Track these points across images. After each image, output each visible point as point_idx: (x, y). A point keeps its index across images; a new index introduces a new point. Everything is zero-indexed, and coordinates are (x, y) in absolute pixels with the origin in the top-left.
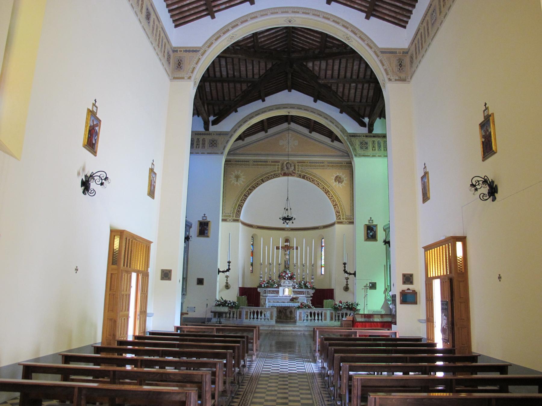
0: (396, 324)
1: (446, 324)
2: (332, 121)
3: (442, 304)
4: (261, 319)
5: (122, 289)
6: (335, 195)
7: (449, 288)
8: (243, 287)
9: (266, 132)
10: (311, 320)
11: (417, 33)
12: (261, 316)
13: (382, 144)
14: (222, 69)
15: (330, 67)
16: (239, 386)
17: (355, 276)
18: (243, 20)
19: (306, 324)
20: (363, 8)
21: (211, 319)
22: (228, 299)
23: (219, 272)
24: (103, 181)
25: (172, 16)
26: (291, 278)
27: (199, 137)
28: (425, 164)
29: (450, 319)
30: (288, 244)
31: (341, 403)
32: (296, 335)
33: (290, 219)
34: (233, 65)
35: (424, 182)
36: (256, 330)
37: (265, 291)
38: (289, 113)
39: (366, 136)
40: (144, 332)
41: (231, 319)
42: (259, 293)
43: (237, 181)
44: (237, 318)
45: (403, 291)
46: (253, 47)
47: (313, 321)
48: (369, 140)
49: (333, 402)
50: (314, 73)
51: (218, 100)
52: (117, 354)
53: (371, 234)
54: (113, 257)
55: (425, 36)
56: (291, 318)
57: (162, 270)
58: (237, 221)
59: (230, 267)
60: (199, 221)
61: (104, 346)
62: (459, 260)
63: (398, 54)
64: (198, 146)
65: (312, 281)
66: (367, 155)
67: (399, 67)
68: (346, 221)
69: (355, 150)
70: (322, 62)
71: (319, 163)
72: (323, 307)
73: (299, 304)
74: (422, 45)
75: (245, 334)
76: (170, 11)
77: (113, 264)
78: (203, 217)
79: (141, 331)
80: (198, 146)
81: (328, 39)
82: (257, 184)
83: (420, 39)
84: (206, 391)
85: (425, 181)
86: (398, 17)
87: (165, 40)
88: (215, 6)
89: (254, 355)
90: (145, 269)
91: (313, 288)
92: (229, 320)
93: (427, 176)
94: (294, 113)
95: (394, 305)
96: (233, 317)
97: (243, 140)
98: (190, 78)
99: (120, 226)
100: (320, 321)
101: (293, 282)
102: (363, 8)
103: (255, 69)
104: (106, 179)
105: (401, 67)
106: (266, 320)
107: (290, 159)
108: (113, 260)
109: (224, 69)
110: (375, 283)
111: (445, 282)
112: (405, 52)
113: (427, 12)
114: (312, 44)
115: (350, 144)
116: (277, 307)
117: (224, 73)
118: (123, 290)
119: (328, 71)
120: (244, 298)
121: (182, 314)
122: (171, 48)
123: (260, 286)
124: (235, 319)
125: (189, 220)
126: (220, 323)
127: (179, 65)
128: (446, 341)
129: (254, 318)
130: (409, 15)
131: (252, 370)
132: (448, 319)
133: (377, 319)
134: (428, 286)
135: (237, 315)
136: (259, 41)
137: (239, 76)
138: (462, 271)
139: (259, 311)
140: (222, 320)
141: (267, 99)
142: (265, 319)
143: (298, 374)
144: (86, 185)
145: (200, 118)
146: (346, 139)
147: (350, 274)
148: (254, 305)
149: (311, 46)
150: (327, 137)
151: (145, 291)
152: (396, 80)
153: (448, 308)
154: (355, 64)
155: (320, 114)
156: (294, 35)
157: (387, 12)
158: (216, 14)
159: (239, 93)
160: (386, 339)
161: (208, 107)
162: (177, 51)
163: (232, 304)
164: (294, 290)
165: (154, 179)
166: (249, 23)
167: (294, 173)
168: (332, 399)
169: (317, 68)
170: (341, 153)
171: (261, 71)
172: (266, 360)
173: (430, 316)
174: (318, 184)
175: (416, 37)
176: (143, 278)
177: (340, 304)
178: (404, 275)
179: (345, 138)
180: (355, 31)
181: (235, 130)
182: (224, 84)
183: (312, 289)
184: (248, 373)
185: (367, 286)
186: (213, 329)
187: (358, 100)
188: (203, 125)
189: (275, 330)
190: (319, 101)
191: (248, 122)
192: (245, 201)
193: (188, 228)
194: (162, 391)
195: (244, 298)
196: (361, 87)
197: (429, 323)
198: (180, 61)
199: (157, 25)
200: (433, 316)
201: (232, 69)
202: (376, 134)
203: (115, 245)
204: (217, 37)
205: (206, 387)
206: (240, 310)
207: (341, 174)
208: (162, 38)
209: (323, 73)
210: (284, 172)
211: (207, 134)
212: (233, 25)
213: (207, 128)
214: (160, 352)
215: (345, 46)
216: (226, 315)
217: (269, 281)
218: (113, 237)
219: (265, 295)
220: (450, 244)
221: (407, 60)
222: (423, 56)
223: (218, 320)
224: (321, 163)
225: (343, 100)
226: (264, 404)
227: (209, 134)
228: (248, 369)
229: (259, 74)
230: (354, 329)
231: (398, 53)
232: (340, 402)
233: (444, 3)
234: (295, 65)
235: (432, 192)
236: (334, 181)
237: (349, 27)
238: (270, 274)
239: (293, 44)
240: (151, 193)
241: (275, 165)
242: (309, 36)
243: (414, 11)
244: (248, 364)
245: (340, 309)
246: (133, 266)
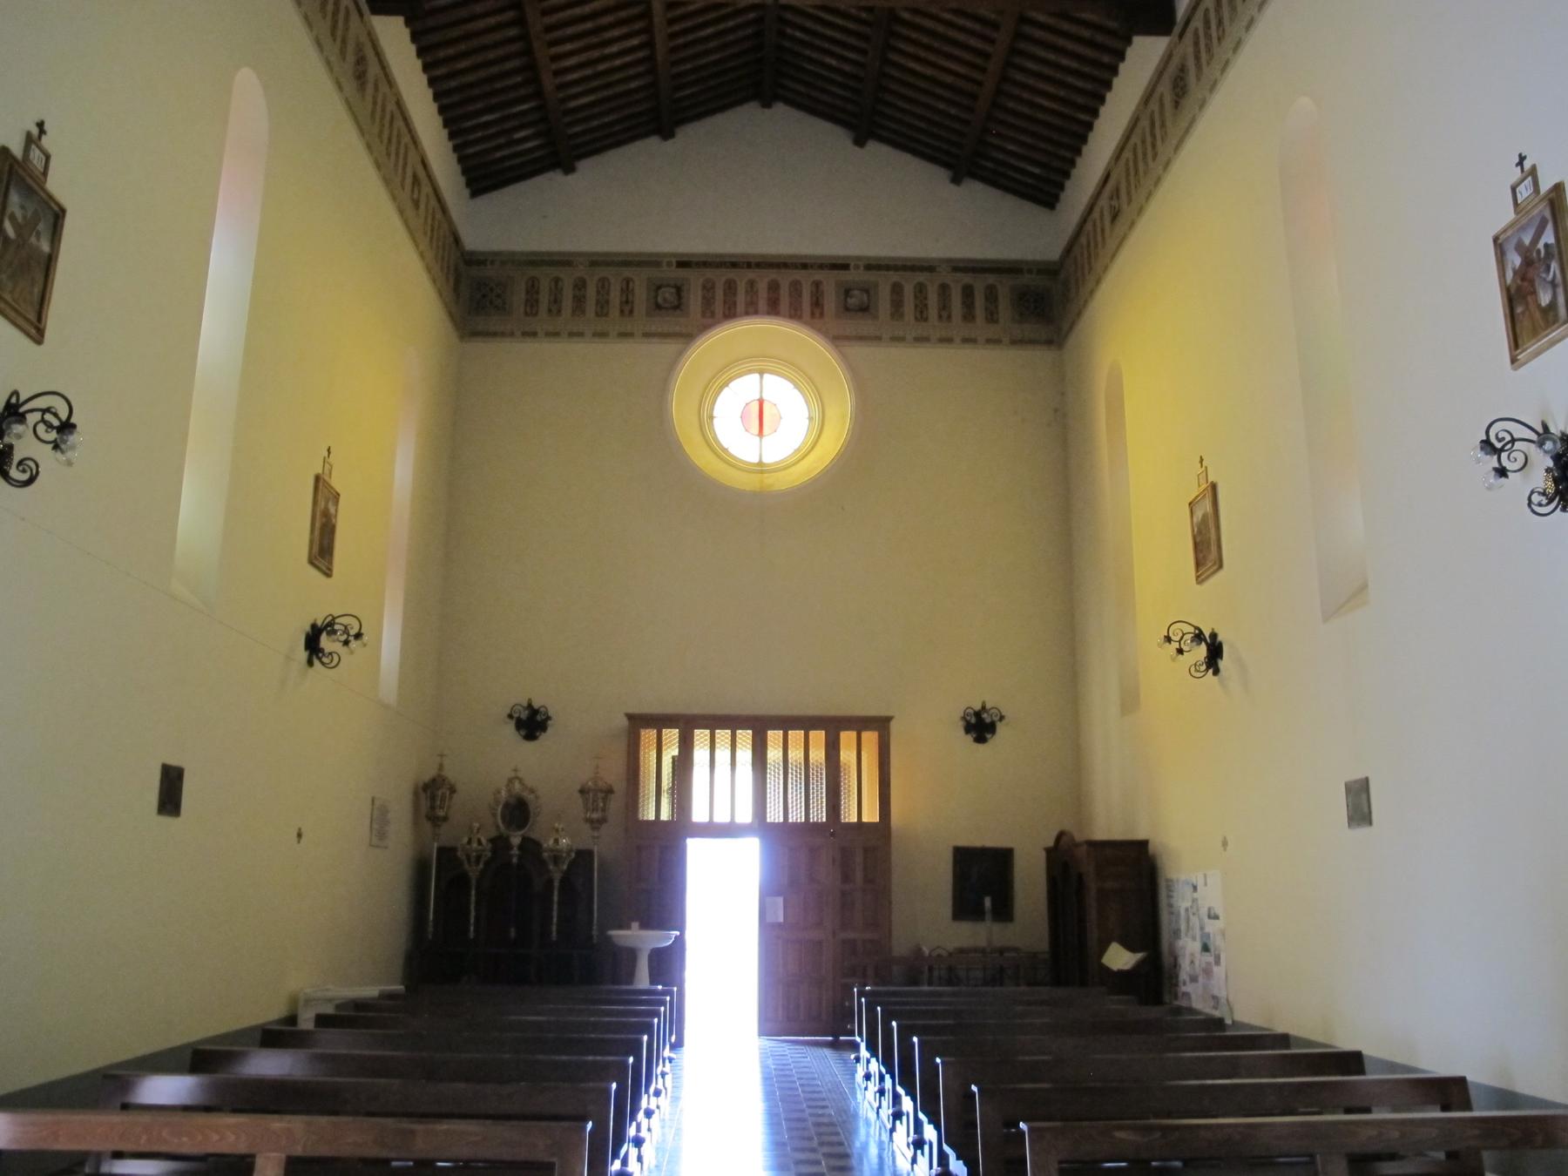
24: (351, 638)
28: (1202, 460)
83: (1148, 130)
87: (406, 139)
144: (313, 643)
233: (1221, 32)
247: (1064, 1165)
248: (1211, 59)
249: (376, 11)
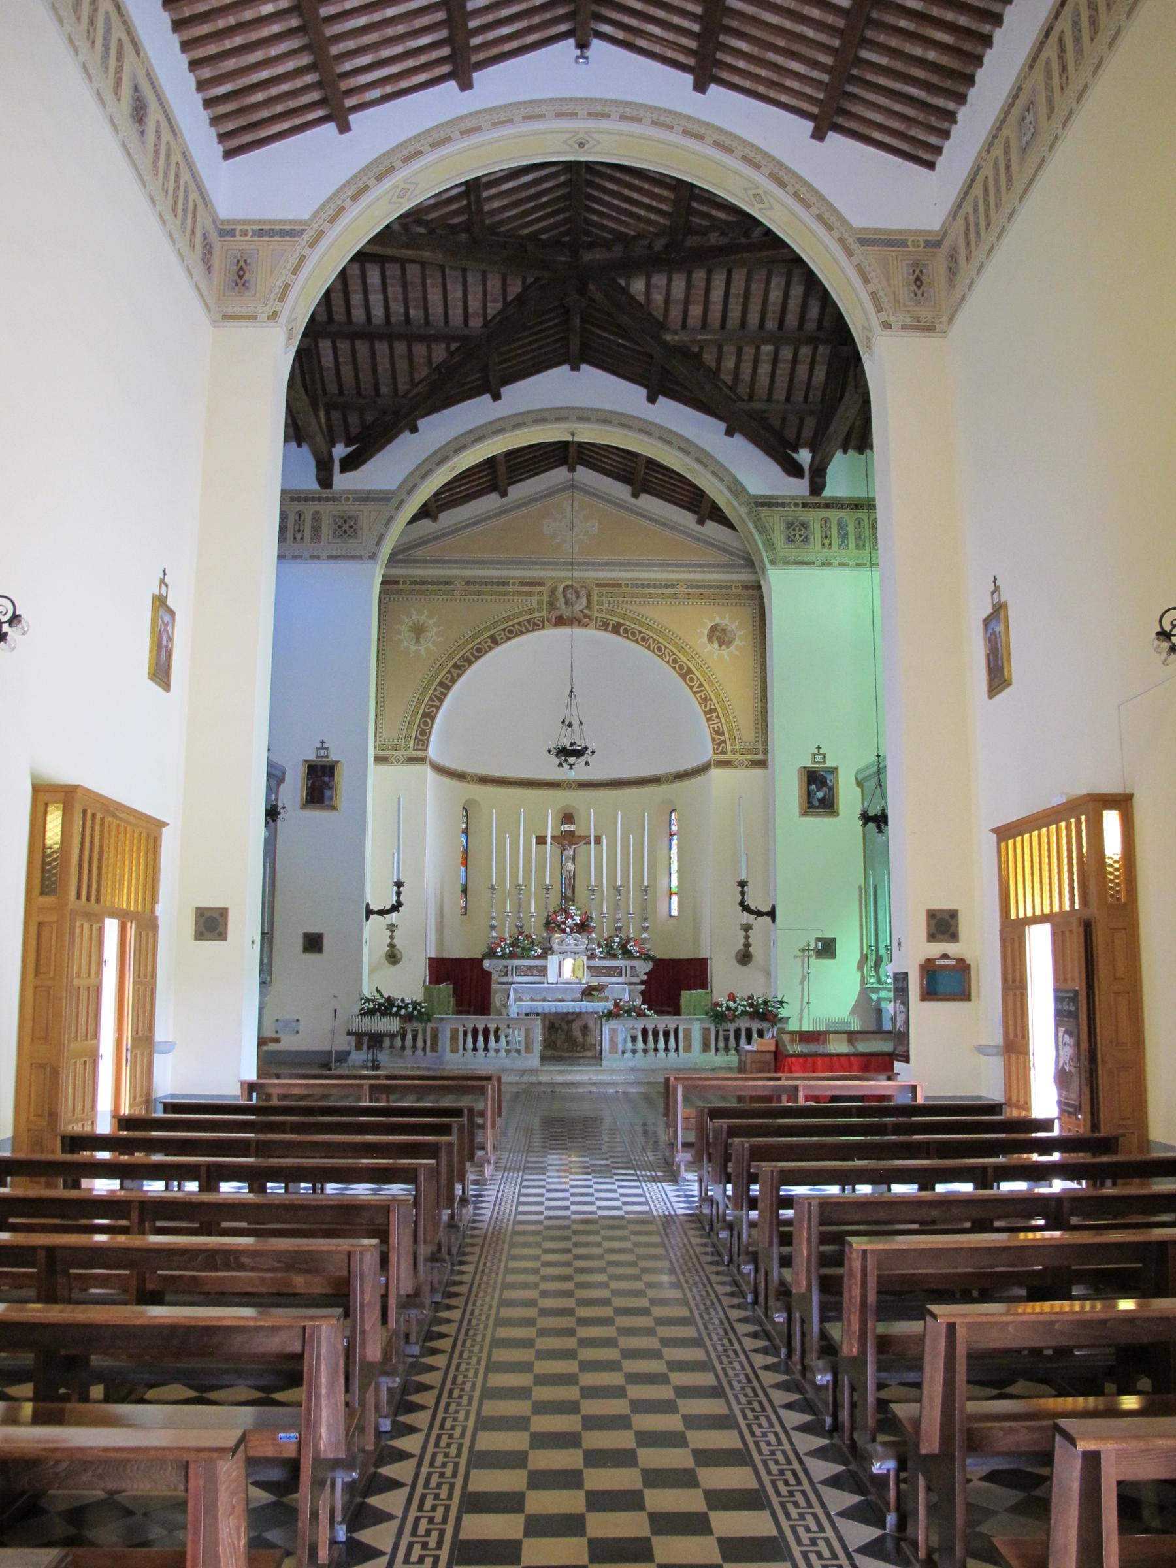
0: (907, 1060)
1: (1071, 1059)
2: (704, 458)
3: (1059, 999)
4: (497, 1051)
5: (76, 970)
6: (710, 683)
7: (1082, 950)
8: (440, 956)
9: (504, 494)
10: (645, 1051)
11: (973, 180)
12: (497, 1040)
13: (851, 529)
14: (372, 297)
15: (698, 293)
16: (453, 1264)
17: (774, 920)
18: (439, 137)
19: (630, 1064)
20: (805, 106)
21: (348, 1053)
22: (396, 995)
23: (369, 912)
25: (215, 121)
26: (583, 927)
27: (300, 507)
28: (995, 579)
29: (1085, 1045)
30: (572, 827)
31: (789, 1319)
32: (604, 1098)
33: (578, 753)
34: (405, 286)
35: (994, 633)
36: (493, 1086)
37: (506, 967)
38: (573, 434)
39: (804, 505)
40: (148, 1101)
41: (408, 1052)
42: (489, 974)
43: (418, 641)
44: (424, 1049)
45: (928, 961)
46: (467, 227)
47: (652, 1053)
48: (814, 517)
49: (754, 1310)
50: (650, 314)
51: (359, 393)
52: (61, 1181)
53: (820, 795)
54: (43, 871)
55: (998, 190)
56: (585, 1047)
57: (198, 909)
58: (420, 760)
59: (402, 899)
60: (306, 761)
61: (22, 1156)
62: (1111, 866)
63: (911, 249)
64: (298, 536)
65: (645, 935)
66: (806, 560)
67: (914, 288)
68: (743, 757)
69: (770, 545)
70: (675, 276)
71: (660, 586)
72: (679, 1014)
73: (610, 1005)
74: (987, 215)
75: (464, 1102)
76: (208, 103)
77: (42, 893)
78: (318, 749)
79: (138, 1099)
80: (298, 536)
81: (695, 205)
82: (479, 650)
84: (362, 1305)
85: (997, 630)
86: (913, 132)
87: (194, 196)
88: (350, 92)
89: (489, 1162)
90: (144, 906)
91: (646, 957)
92: (401, 1057)
93: (1002, 615)
94: (589, 434)
95: (902, 1003)
96: (414, 1047)
97: (435, 519)
98: (274, 316)
99: (64, 773)
100: (672, 1054)
101: (589, 939)
102: (805, 106)
103: (470, 297)
104: (15, 621)
105: (919, 287)
106: (514, 1054)
107: (576, 574)
108: (43, 879)
109: (376, 299)
110: (833, 940)
111: (1067, 933)
112: (933, 243)
113: (1007, 113)
114: (649, 222)
115: (756, 526)
116: (545, 1014)
117: (378, 312)
118: (79, 973)
119: (691, 307)
120: (446, 988)
121: (262, 1041)
122: (214, 222)
123: (491, 954)
124: (419, 1052)
125: (275, 759)
126: (376, 1067)
127: (241, 277)
128: (1070, 1109)
129: (475, 1049)
130: (945, 125)
131: (487, 1211)
132: (1078, 1044)
133: (838, 1046)
134: (1009, 945)
135: (425, 1042)
136: (486, 208)
137: (422, 321)
138: (1119, 899)
139: (492, 1027)
140: (383, 1057)
141: (506, 391)
142: (508, 1051)
143: (630, 1222)
145: (305, 450)
146: (744, 515)
147: (759, 914)
148: (472, 1009)
149: (642, 225)
150: (683, 511)
151: (145, 976)
152: (904, 327)
153: (1077, 1009)
154: (772, 285)
155: (667, 437)
156: (589, 190)
157: (878, 117)
158: (352, 118)
159: (424, 374)
160: (879, 1106)
161: (327, 414)
162: (231, 233)
163: (410, 1010)
164: (592, 963)
165: (169, 628)
166: (458, 147)
167: (586, 616)
168: (749, 1300)
169: (658, 297)
170: (725, 558)
171: (489, 305)
172: (526, 1177)
173: (1016, 1036)
174: (659, 649)
175: (966, 193)
176: (139, 934)
177: (731, 1004)
178: (932, 915)
179: (743, 510)
180: (781, 175)
181: (409, 484)
182: (377, 345)
183: (645, 960)
184: (475, 1221)
185: (808, 950)
186: (361, 1086)
187: (780, 395)
188: (314, 471)
189: (540, 1083)
190: (662, 399)
191: (451, 463)
192: (441, 701)
193: (273, 783)
194: (219, 1323)
195: (446, 988)
196: (790, 357)
197: (1013, 1056)
198: (242, 263)
199: (168, 143)
200: (1025, 1036)
201: (400, 297)
202: (832, 498)
203: (48, 834)
204: (357, 188)
205: (362, 1292)
206: (434, 1025)
207: (726, 621)
208: (186, 187)
209: (675, 313)
210: (558, 613)
211: (327, 499)
212: (406, 153)
213: (325, 481)
214: (203, 1170)
215: (747, 221)
216: (392, 1042)
217: (517, 939)
218: (41, 808)
219: (504, 979)
220: (1083, 818)
221: (938, 268)
222: (992, 248)
223: (370, 1057)
224: (666, 586)
225: (736, 394)
226: (539, 1326)
227: (333, 499)
228: (476, 1208)
229: (485, 315)
230: (788, 1079)
231: (909, 244)
232: (785, 1315)
233: (1064, 79)
234: (591, 287)
235: (1018, 666)
236: (705, 639)
237: (763, 162)
238: (519, 918)
239: (588, 221)
240: (161, 673)
241: (530, 594)
242: (636, 196)
243: (963, 113)
244: (472, 1190)
245: (729, 1014)
246: (109, 898)
247: (888, 1298)
248: (1096, 33)
249: (775, 1538)
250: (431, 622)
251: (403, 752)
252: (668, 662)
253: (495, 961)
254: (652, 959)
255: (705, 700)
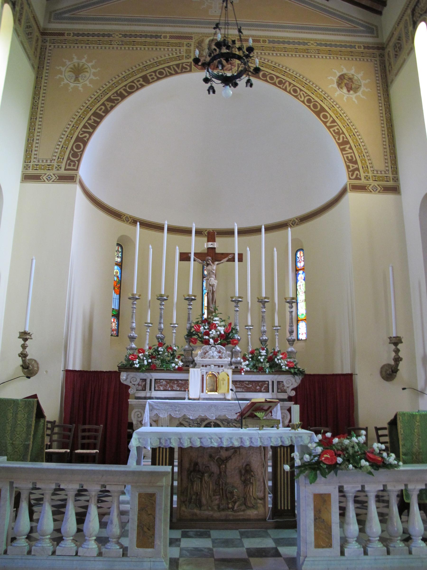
37: (145, 380)
43: (76, 79)
58: (71, 179)
68: (376, 183)
82: (131, 87)
164: (238, 377)
170: (348, 25)
174: (295, 91)
192: (94, 128)
207: (352, 72)
217: (157, 351)
219: (142, 394)
224: (299, 43)
236: (335, 85)
238: (160, 330)
241: (180, 45)
250: (90, 64)
251: (55, 171)
252: (303, 102)
253: (132, 374)
254: (301, 372)
255: (338, 133)
